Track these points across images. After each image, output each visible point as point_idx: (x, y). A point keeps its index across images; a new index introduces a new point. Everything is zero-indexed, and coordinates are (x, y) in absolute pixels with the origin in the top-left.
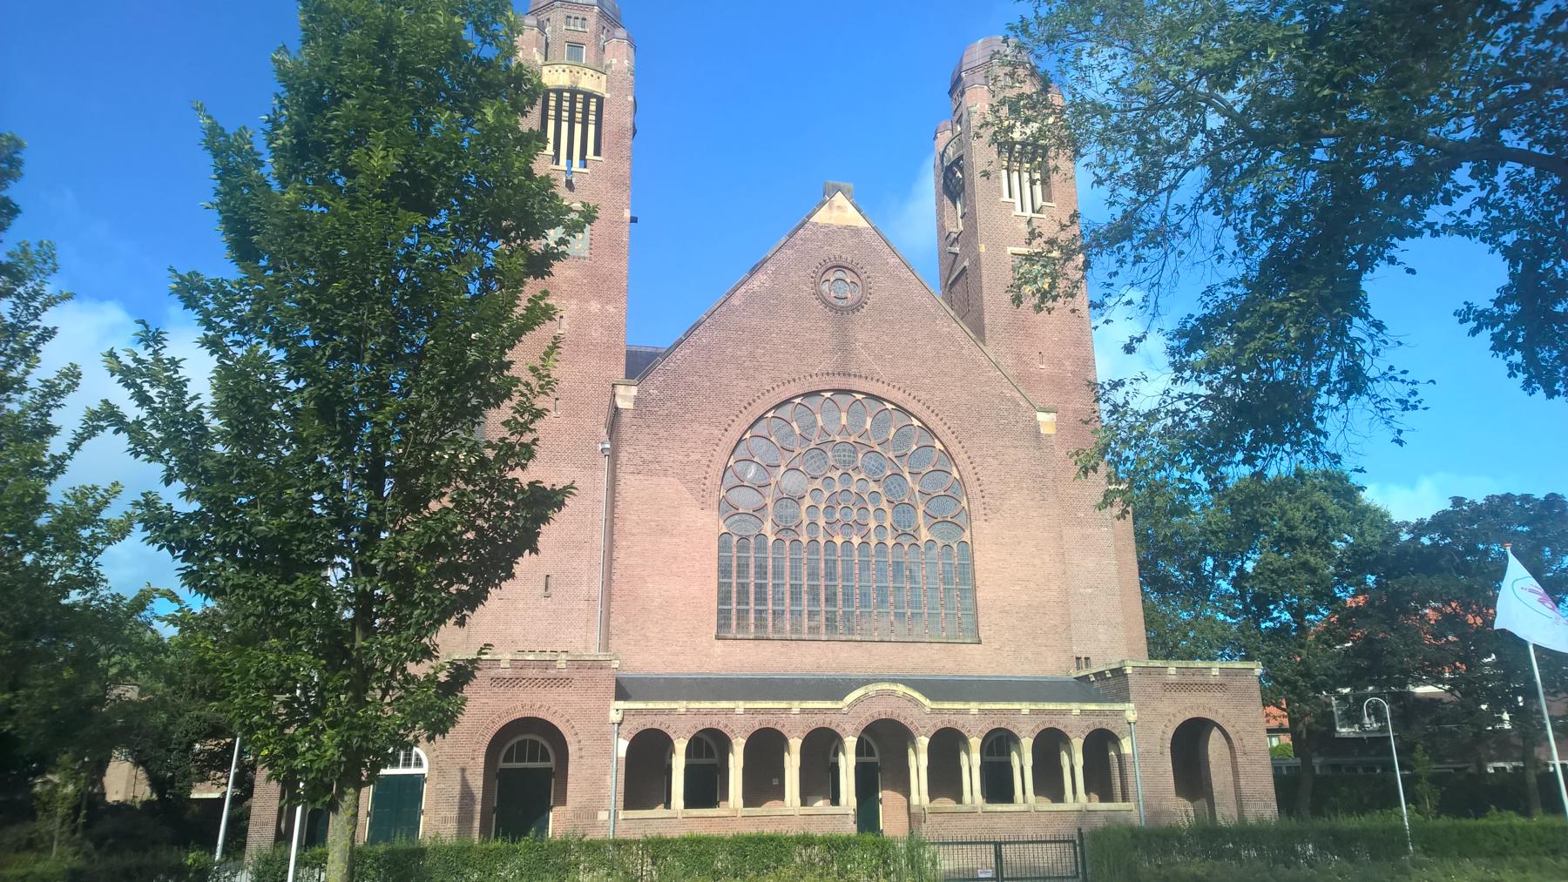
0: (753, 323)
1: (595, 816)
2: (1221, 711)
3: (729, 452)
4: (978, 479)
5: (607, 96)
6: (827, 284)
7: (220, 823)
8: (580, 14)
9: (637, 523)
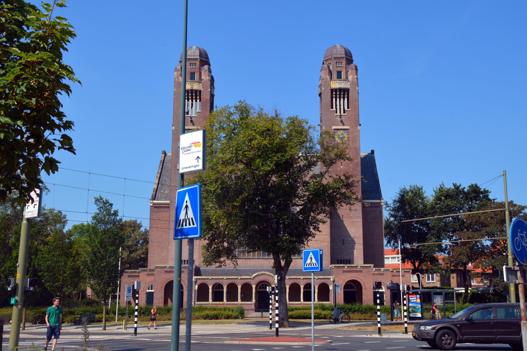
2: (360, 278)
5: (202, 90)
8: (194, 62)
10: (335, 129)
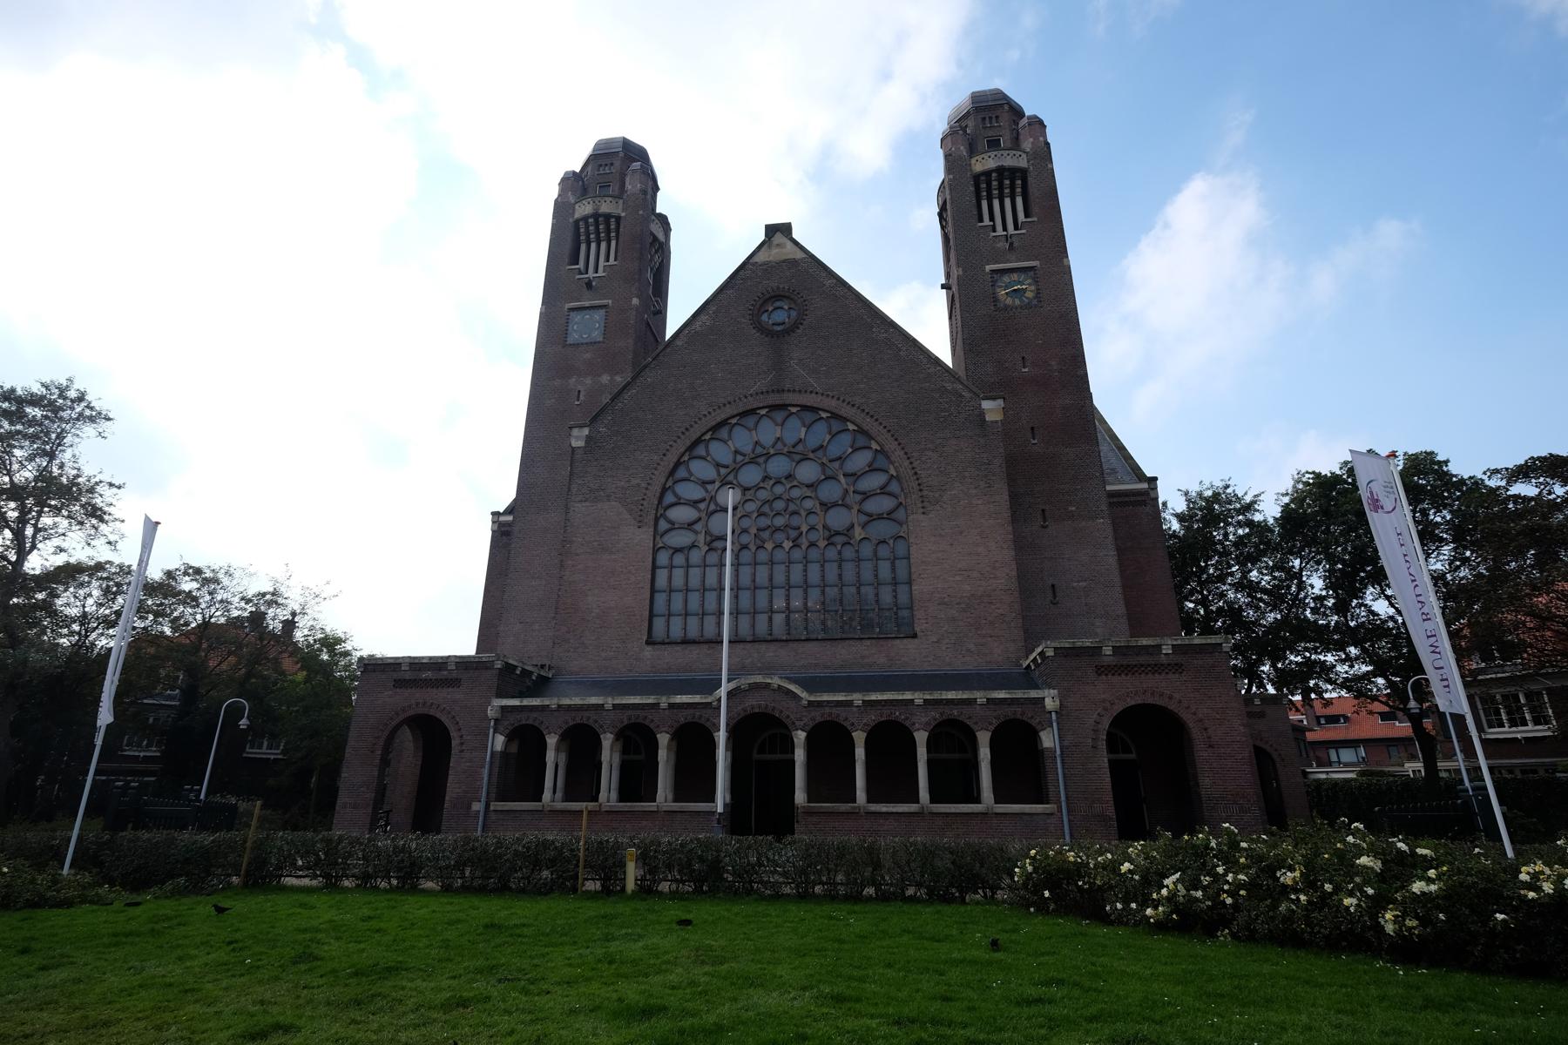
0: (694, 359)
1: (469, 807)
2: (1177, 696)
3: (666, 474)
4: (916, 473)
5: (623, 214)
6: (766, 315)
7: (1449, 727)
9: (582, 545)
10: (993, 271)
